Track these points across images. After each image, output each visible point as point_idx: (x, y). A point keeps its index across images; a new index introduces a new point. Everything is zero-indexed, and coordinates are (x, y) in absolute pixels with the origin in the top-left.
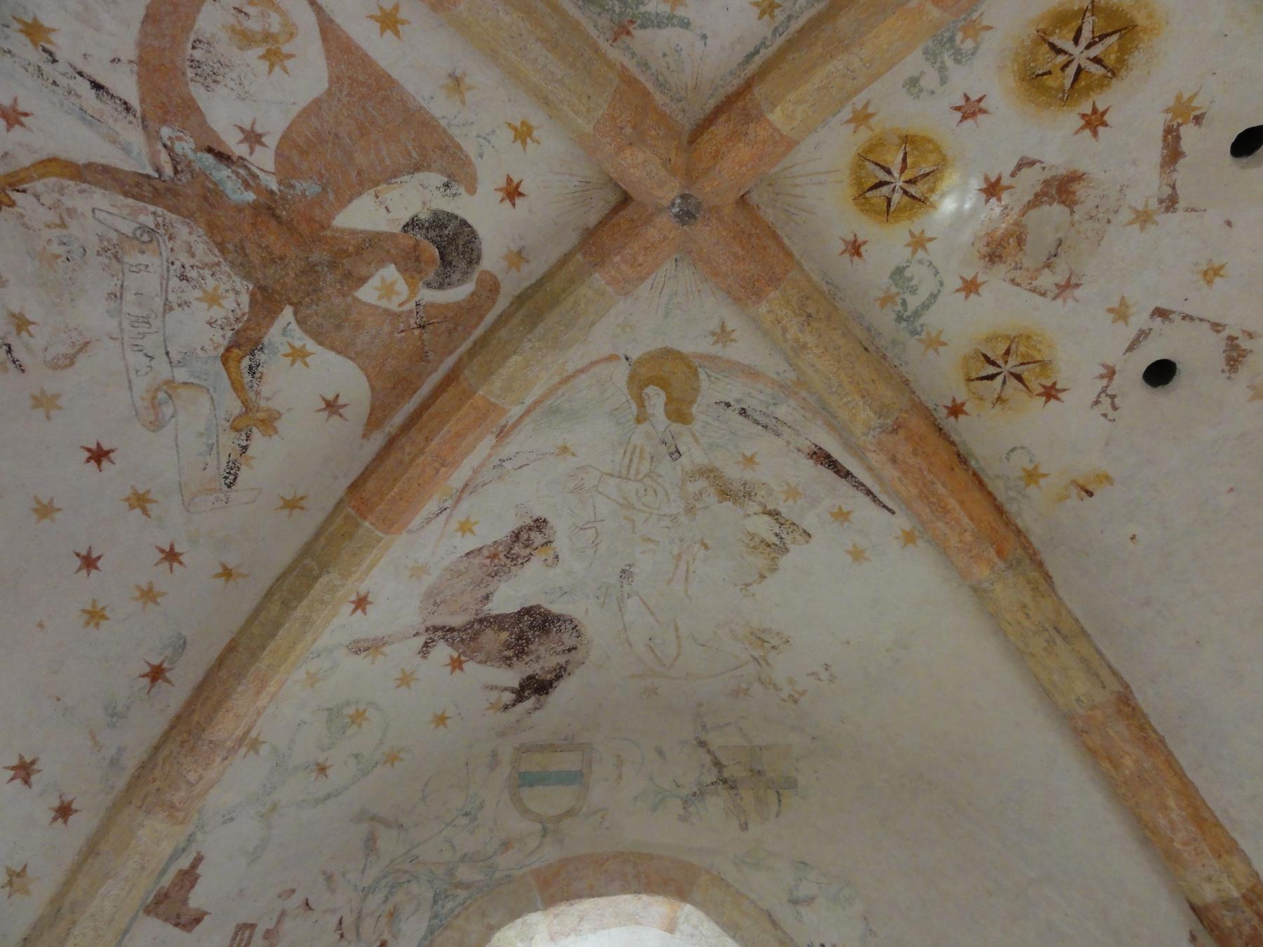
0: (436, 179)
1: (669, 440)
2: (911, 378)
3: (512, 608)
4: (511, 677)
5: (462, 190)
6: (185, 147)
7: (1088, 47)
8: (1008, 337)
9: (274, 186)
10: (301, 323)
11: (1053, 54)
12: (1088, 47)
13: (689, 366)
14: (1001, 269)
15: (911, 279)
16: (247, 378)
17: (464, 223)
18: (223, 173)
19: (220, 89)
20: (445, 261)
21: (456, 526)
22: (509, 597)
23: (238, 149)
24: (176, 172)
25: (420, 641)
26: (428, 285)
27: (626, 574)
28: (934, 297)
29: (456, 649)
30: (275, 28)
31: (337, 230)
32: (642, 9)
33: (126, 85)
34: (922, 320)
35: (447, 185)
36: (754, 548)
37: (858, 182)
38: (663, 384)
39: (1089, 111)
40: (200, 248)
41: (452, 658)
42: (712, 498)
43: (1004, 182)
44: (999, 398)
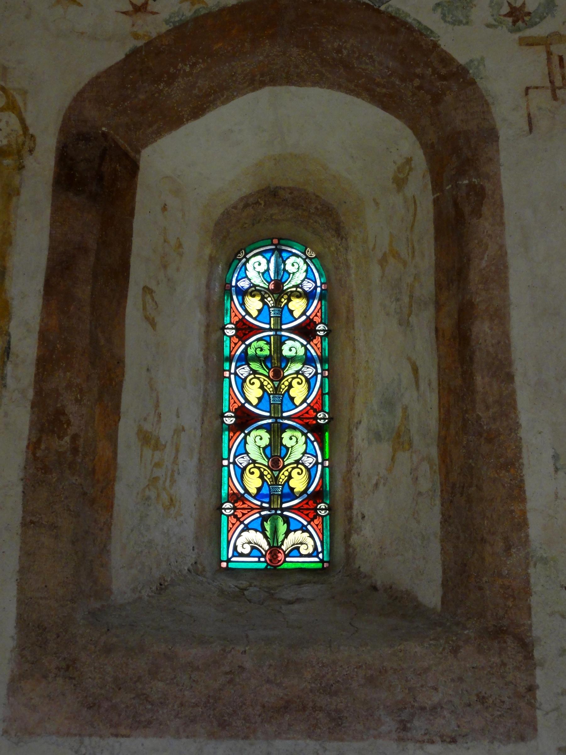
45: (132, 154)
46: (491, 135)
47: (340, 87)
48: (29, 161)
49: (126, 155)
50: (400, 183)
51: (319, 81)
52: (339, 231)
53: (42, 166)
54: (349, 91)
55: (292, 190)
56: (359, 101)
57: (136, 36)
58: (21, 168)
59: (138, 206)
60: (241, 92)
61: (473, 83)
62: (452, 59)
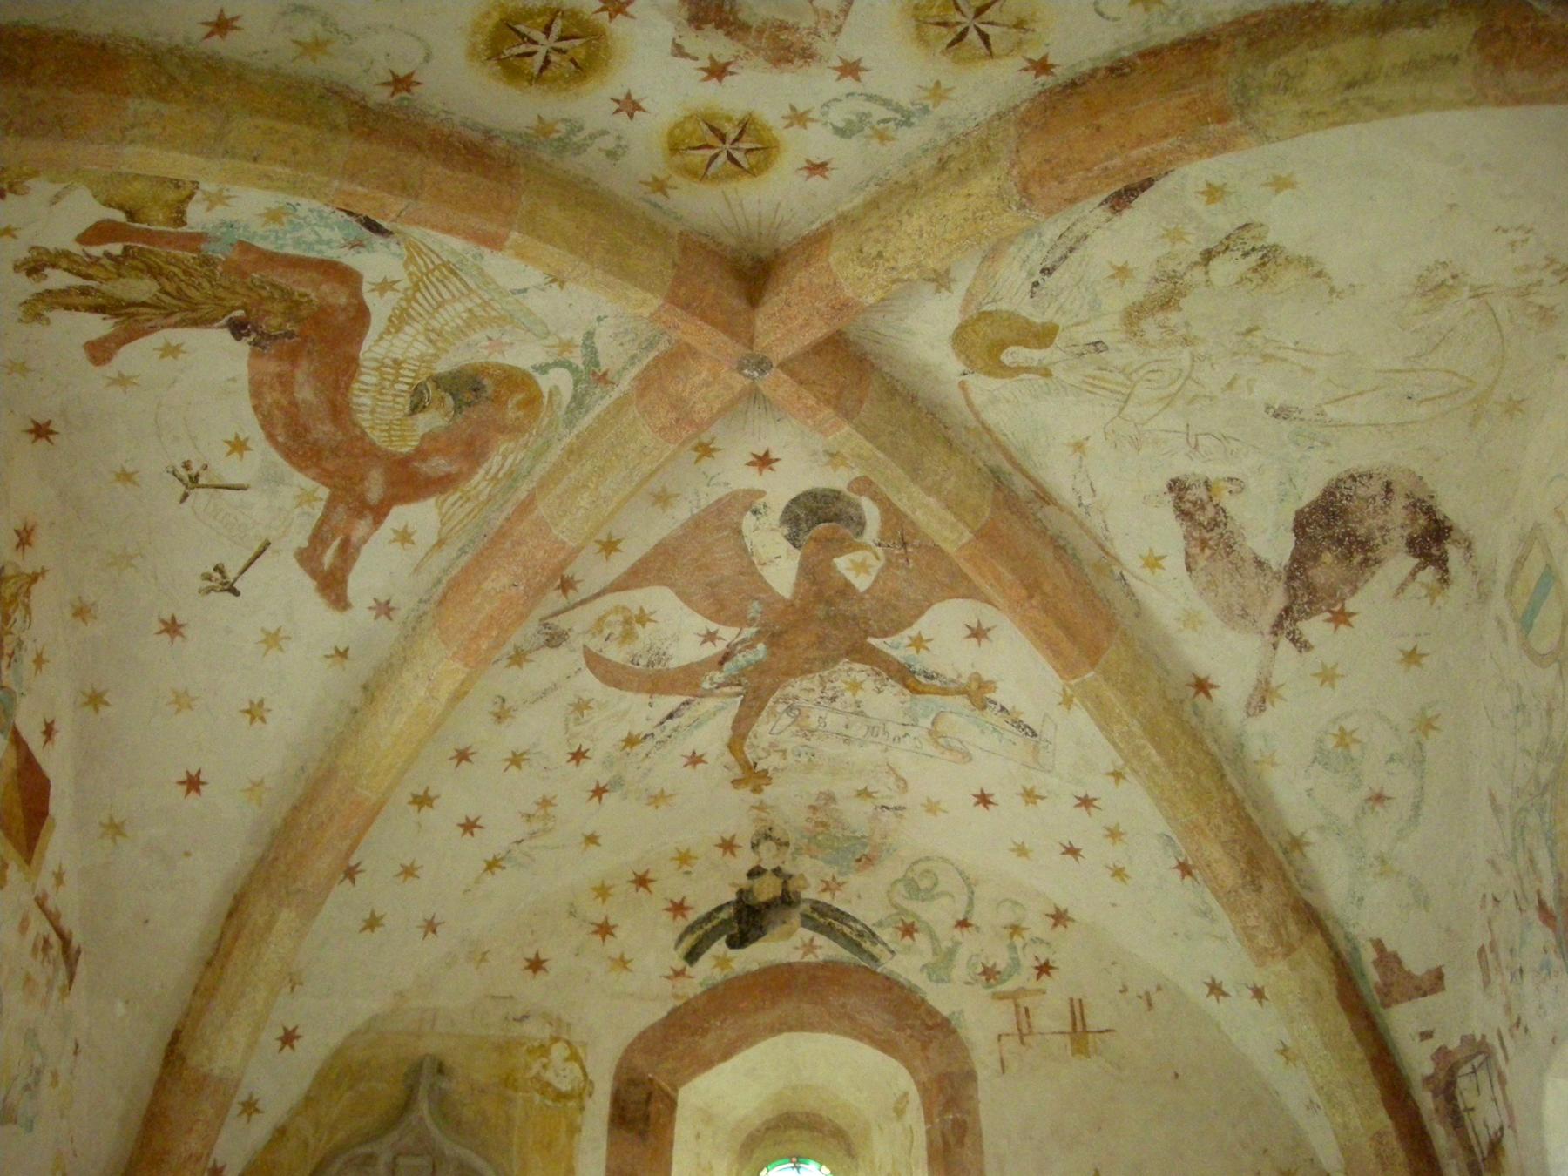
0: (748, 521)
1: (195, 468)
2: (993, 111)
3: (1288, 543)
4: (1398, 564)
5: (761, 501)
6: (719, 677)
7: (535, 43)
8: (918, 28)
9: (753, 630)
10: (886, 634)
11: (552, 66)
12: (535, 43)
13: (979, 319)
14: (820, 46)
15: (850, 122)
16: (936, 682)
17: (795, 501)
18: (740, 659)
19: (671, 651)
20: (836, 518)
21: (1148, 571)
22: (1273, 542)
23: (720, 647)
24: (740, 684)
25: (1284, 643)
26: (860, 534)
27: (1281, 413)
28: (870, 98)
29: (1320, 611)
30: (620, 617)
31: (796, 593)
32: (582, 367)
33: (673, 701)
34: (905, 102)
35: (755, 512)
36: (1265, 279)
37: (729, 177)
38: (1003, 345)
39: (606, 15)
40: (806, 684)
41: (1329, 620)
42: (1174, 318)
43: (707, 64)
44: (1016, 26)
45: (672, 1093)
46: (971, 1076)
47: (845, 1034)
48: (588, 1103)
49: (668, 1095)
50: (899, 1113)
51: (828, 1028)
52: (850, 1152)
53: (599, 1107)
54: (856, 1038)
55: (807, 1115)
56: (861, 1045)
57: (676, 996)
58: (582, 1109)
59: (676, 1137)
60: (764, 1038)
61: (954, 1032)
62: (937, 1013)
